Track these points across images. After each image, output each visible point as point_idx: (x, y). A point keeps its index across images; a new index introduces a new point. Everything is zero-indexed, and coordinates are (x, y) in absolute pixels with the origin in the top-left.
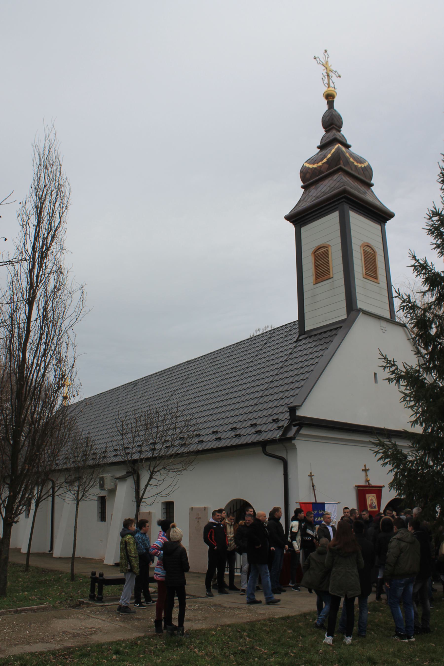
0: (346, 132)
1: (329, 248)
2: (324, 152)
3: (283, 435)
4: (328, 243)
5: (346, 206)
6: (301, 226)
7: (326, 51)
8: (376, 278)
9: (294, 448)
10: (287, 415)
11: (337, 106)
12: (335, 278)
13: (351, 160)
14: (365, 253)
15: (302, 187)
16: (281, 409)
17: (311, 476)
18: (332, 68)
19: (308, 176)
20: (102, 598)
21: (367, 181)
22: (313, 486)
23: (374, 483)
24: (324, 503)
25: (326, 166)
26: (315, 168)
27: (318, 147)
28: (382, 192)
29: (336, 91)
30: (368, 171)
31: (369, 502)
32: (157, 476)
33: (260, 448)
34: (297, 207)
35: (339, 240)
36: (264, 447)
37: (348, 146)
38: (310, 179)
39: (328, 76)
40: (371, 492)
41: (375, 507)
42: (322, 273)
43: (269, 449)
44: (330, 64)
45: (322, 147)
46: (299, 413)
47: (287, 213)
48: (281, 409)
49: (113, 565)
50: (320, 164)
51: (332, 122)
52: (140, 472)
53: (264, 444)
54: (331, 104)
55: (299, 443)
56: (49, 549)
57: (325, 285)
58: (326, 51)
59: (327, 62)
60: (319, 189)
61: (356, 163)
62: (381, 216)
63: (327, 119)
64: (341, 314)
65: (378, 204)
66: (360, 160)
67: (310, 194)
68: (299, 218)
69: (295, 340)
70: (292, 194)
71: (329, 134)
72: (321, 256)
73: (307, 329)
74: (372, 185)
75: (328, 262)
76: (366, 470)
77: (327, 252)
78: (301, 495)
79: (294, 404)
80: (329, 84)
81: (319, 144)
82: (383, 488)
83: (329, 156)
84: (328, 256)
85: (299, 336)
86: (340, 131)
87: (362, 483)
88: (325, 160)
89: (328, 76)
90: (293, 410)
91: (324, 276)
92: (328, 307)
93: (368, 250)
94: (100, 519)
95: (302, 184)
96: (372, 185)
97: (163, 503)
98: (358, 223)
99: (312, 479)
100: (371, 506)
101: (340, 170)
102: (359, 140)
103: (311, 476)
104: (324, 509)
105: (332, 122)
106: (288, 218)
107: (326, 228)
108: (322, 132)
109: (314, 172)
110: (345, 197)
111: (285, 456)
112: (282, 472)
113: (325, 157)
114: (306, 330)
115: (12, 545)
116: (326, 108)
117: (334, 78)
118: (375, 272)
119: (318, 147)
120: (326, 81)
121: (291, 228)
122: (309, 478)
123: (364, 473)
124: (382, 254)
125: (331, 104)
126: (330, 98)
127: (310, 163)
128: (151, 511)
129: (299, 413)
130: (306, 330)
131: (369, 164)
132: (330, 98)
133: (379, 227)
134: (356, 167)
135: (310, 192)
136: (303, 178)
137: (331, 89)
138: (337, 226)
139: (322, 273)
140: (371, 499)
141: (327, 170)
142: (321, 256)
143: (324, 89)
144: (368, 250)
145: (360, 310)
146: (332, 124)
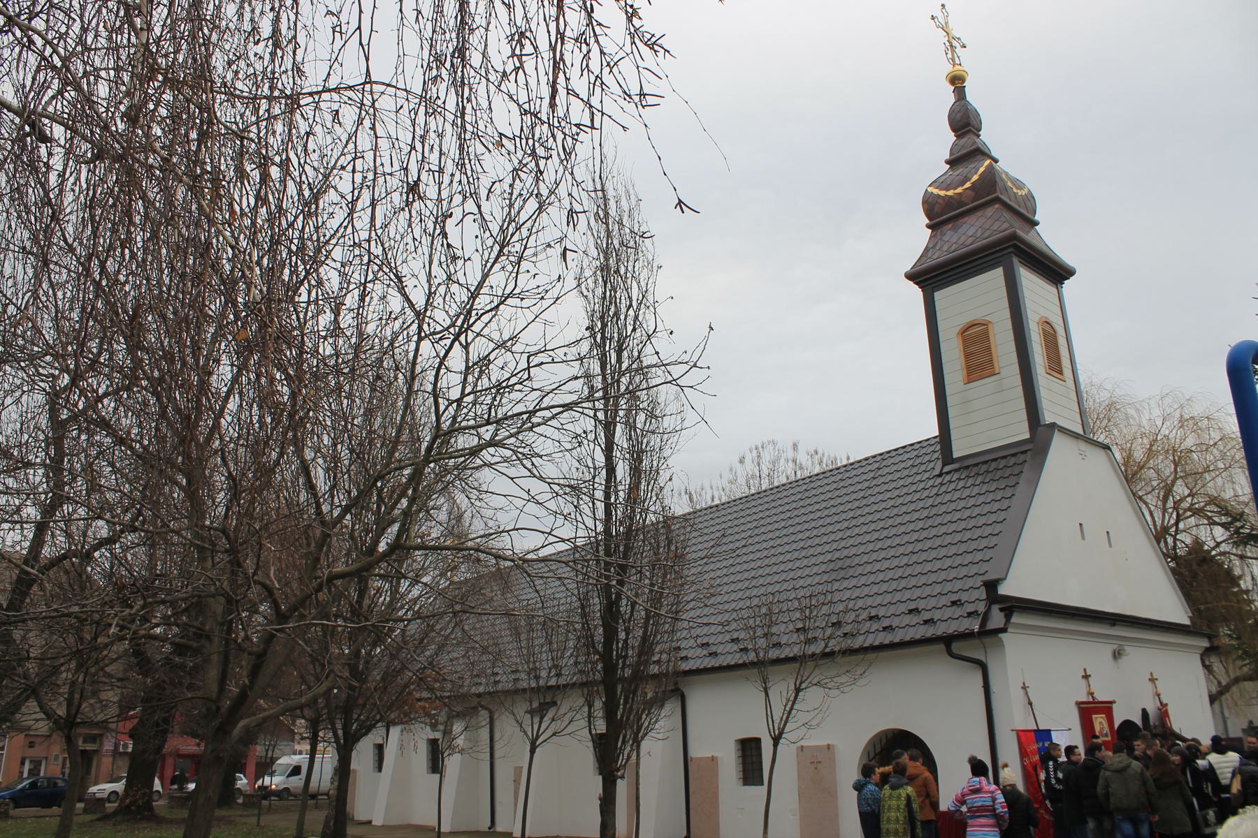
0: (989, 136)
2: (961, 170)
4: (987, 318)
5: (1015, 260)
7: (943, 6)
8: (1061, 373)
9: (1001, 644)
10: (982, 593)
11: (970, 96)
12: (1004, 372)
13: (1009, 184)
14: (1045, 333)
15: (928, 226)
16: (970, 583)
17: (1024, 688)
18: (955, 33)
19: (937, 208)
22: (1030, 704)
23: (1100, 697)
24: (1049, 731)
28: (1052, 234)
31: (1097, 728)
32: (812, 697)
33: (942, 647)
37: (996, 161)
38: (941, 213)
40: (1098, 711)
42: (979, 363)
43: (956, 647)
44: (951, 25)
45: (953, 163)
46: (1003, 590)
48: (970, 583)
50: (959, 190)
51: (964, 122)
53: (947, 641)
54: (960, 93)
55: (1009, 639)
56: (489, 824)
57: (985, 386)
58: (943, 6)
59: (947, 23)
62: (1056, 273)
63: (958, 116)
67: (946, 238)
68: (929, 278)
69: (937, 472)
70: (913, 238)
71: (964, 140)
72: (976, 340)
73: (955, 455)
74: (1037, 224)
75: (989, 348)
76: (1086, 677)
78: (1013, 718)
80: (953, 60)
81: (947, 157)
83: (975, 178)
88: (968, 185)
90: (991, 586)
92: (991, 421)
93: (1048, 329)
95: (927, 221)
98: (1031, 283)
99: (1027, 693)
101: (998, 200)
102: (1012, 149)
103: (1024, 688)
104: (1050, 738)
105: (964, 122)
106: (911, 276)
107: (980, 296)
108: (951, 137)
109: (950, 203)
110: (1015, 246)
111: (982, 658)
113: (967, 179)
116: (951, 99)
117: (959, 50)
118: (1059, 363)
119: (947, 162)
120: (950, 56)
122: (1022, 692)
123: (1084, 681)
124: (1008, 324)
125: (960, 93)
126: (957, 81)
128: (715, 755)
129: (1003, 590)
132: (957, 81)
133: (1053, 289)
135: (943, 234)
136: (929, 213)
137: (958, 67)
138: (1003, 292)
140: (1099, 721)
143: (948, 68)
144: (1048, 329)
145: (1053, 426)
146: (968, 125)
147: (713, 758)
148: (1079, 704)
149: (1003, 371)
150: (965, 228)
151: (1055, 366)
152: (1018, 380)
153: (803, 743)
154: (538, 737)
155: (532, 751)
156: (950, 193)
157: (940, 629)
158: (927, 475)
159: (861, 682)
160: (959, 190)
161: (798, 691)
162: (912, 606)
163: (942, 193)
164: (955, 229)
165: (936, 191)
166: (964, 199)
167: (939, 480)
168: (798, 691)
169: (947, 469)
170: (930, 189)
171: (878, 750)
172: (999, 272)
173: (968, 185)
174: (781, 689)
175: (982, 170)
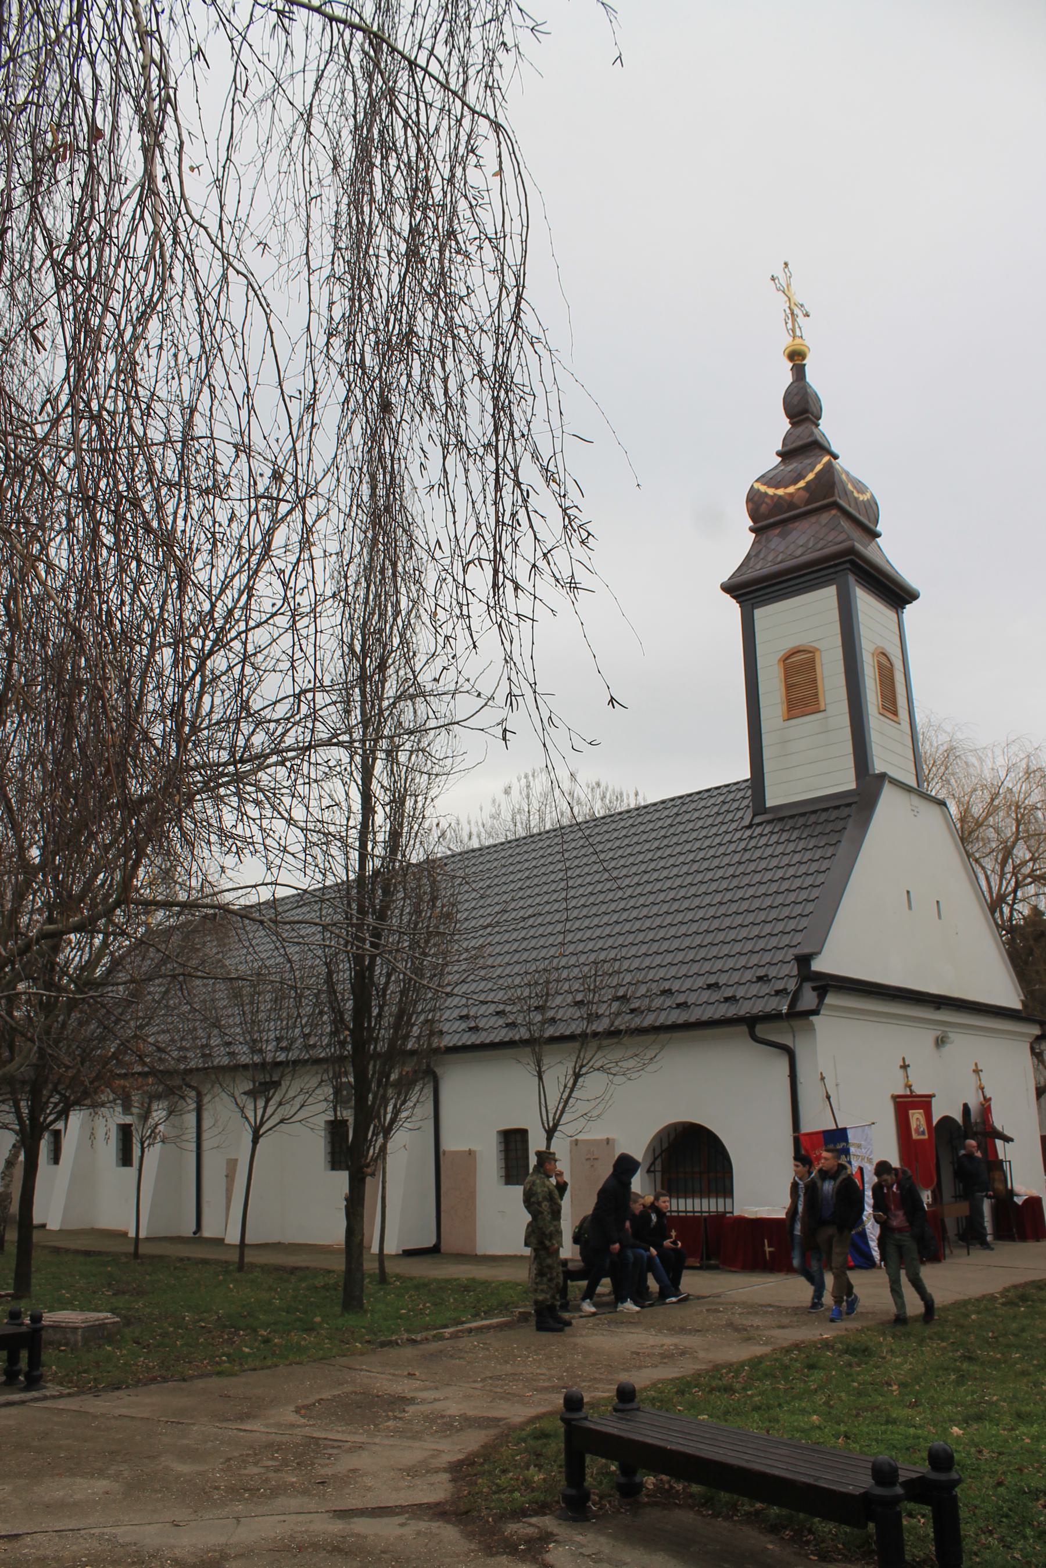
0: (829, 428)
1: (817, 654)
3: (786, 1004)
4: (814, 644)
5: (851, 579)
6: (754, 607)
7: (786, 264)
8: (895, 713)
9: (811, 1028)
13: (850, 487)
14: (880, 666)
15: (752, 530)
19: (763, 509)
20: (567, 1304)
21: (872, 526)
22: (828, 1098)
23: (919, 1090)
25: (805, 495)
26: (780, 497)
27: (779, 454)
28: (896, 549)
29: (806, 343)
30: (872, 508)
31: (914, 1125)
32: (593, 1084)
33: (744, 1029)
34: (745, 569)
35: (838, 641)
36: (751, 1025)
38: (767, 516)
39: (792, 314)
40: (915, 1106)
41: (923, 1133)
42: (802, 698)
43: (760, 1030)
45: (786, 455)
47: (726, 573)
49: (398, 1255)
50: (791, 489)
51: (802, 407)
52: (438, 1070)
53: (751, 1023)
54: (799, 372)
56: (194, 1228)
57: (808, 723)
58: (786, 264)
60: (790, 538)
61: (856, 494)
62: (897, 595)
64: (848, 782)
65: (888, 568)
66: (862, 488)
68: (750, 590)
69: (746, 822)
70: (735, 543)
72: (800, 668)
73: (769, 804)
74: (878, 535)
75: (815, 680)
76: (977, 1071)
77: (813, 661)
79: (806, 950)
80: (793, 331)
81: (780, 448)
82: (933, 1100)
83: (811, 476)
84: (814, 668)
85: (754, 816)
86: (817, 425)
87: (900, 1091)
88: (802, 484)
89: (792, 314)
90: (804, 961)
91: (806, 705)
92: (811, 766)
94: (329, 1166)
95: (751, 524)
96: (878, 535)
97: (499, 1132)
100: (917, 1130)
105: (802, 407)
106: (729, 588)
107: (806, 618)
108: (785, 425)
109: (780, 505)
110: (851, 562)
111: (790, 1044)
112: (787, 1072)
114: (768, 805)
115: (37, 1220)
116: (788, 379)
117: (801, 319)
119: (779, 454)
120: (790, 326)
121: (732, 609)
125: (799, 372)
126: (797, 357)
127: (768, 484)
128: (473, 1148)
130: (768, 805)
131: (872, 496)
132: (797, 357)
133: (891, 614)
134: (856, 499)
135: (768, 541)
136: (754, 515)
137: (798, 341)
138: (835, 615)
139: (802, 698)
140: (916, 1118)
141: (807, 503)
142: (800, 668)
145: (883, 776)
146: (806, 411)
147: (470, 1152)
148: (895, 1098)
149: (829, 708)
150: (794, 535)
151: (889, 705)
152: (844, 707)
153: (579, 1137)
154: (262, 1124)
155: (255, 1141)
156: (780, 492)
157: (744, 1009)
158: (734, 826)
159: (651, 1068)
160: (791, 489)
161: (577, 1076)
162: (712, 980)
163: (771, 491)
164: (783, 535)
165: (763, 489)
166: (795, 500)
167: (748, 833)
168: (577, 1076)
169: (757, 820)
170: (757, 486)
171: (665, 1146)
172: (831, 591)
173: (802, 484)
174: (558, 1071)
175: (819, 467)
